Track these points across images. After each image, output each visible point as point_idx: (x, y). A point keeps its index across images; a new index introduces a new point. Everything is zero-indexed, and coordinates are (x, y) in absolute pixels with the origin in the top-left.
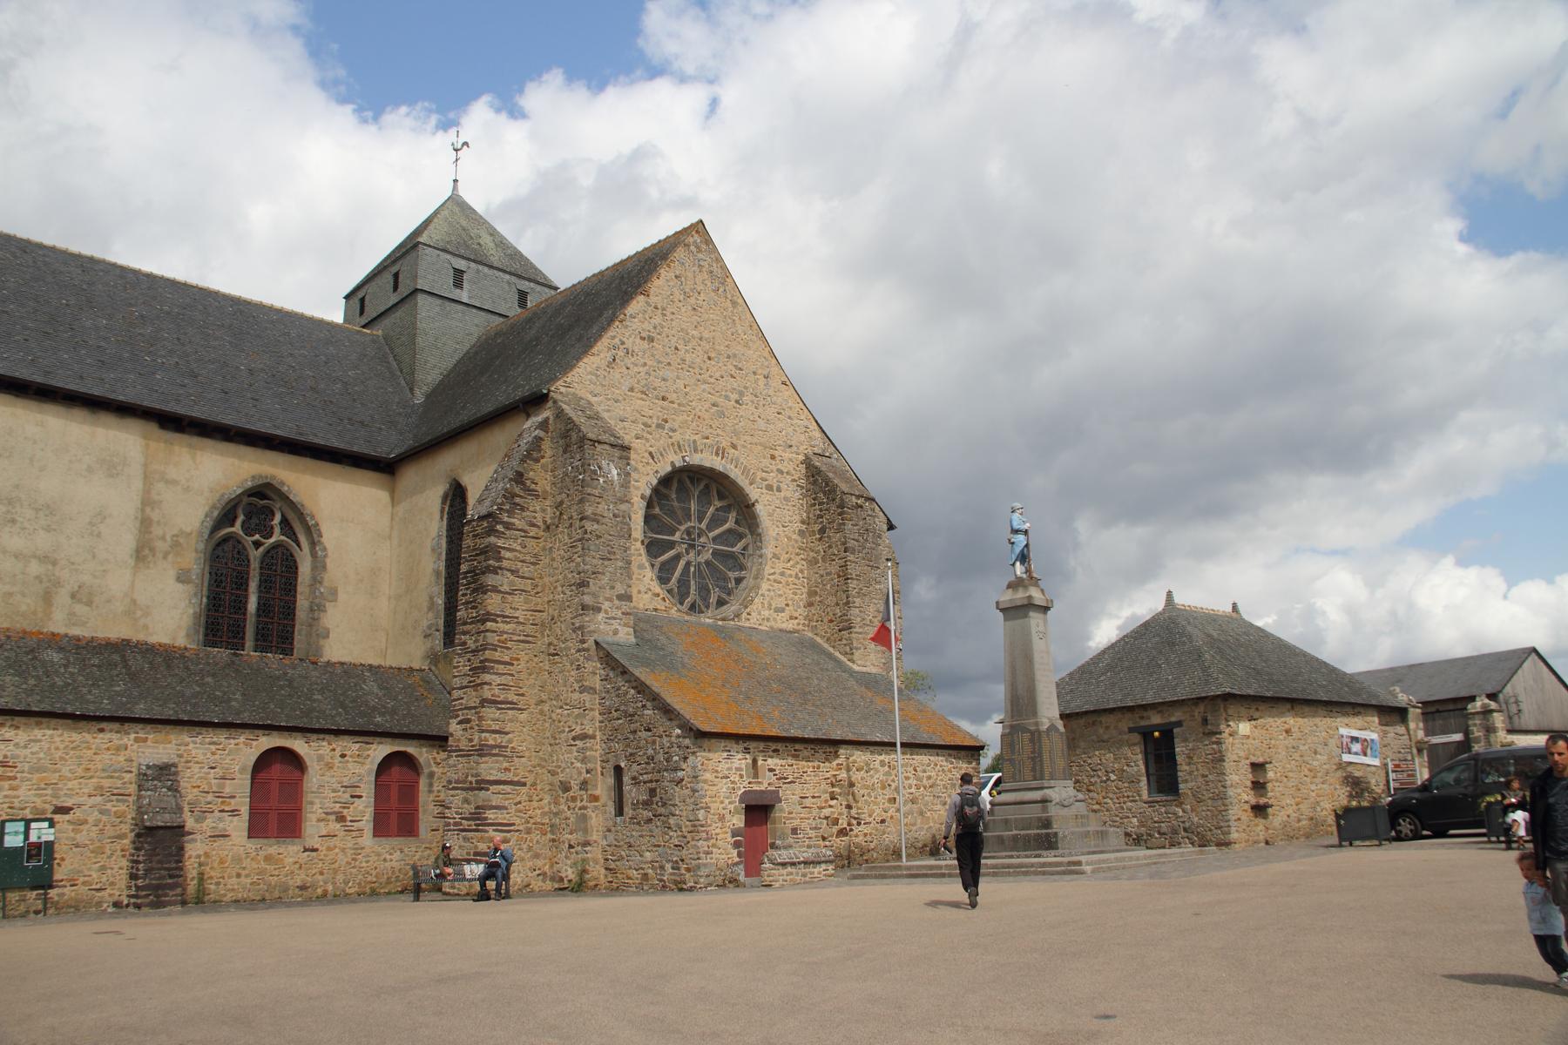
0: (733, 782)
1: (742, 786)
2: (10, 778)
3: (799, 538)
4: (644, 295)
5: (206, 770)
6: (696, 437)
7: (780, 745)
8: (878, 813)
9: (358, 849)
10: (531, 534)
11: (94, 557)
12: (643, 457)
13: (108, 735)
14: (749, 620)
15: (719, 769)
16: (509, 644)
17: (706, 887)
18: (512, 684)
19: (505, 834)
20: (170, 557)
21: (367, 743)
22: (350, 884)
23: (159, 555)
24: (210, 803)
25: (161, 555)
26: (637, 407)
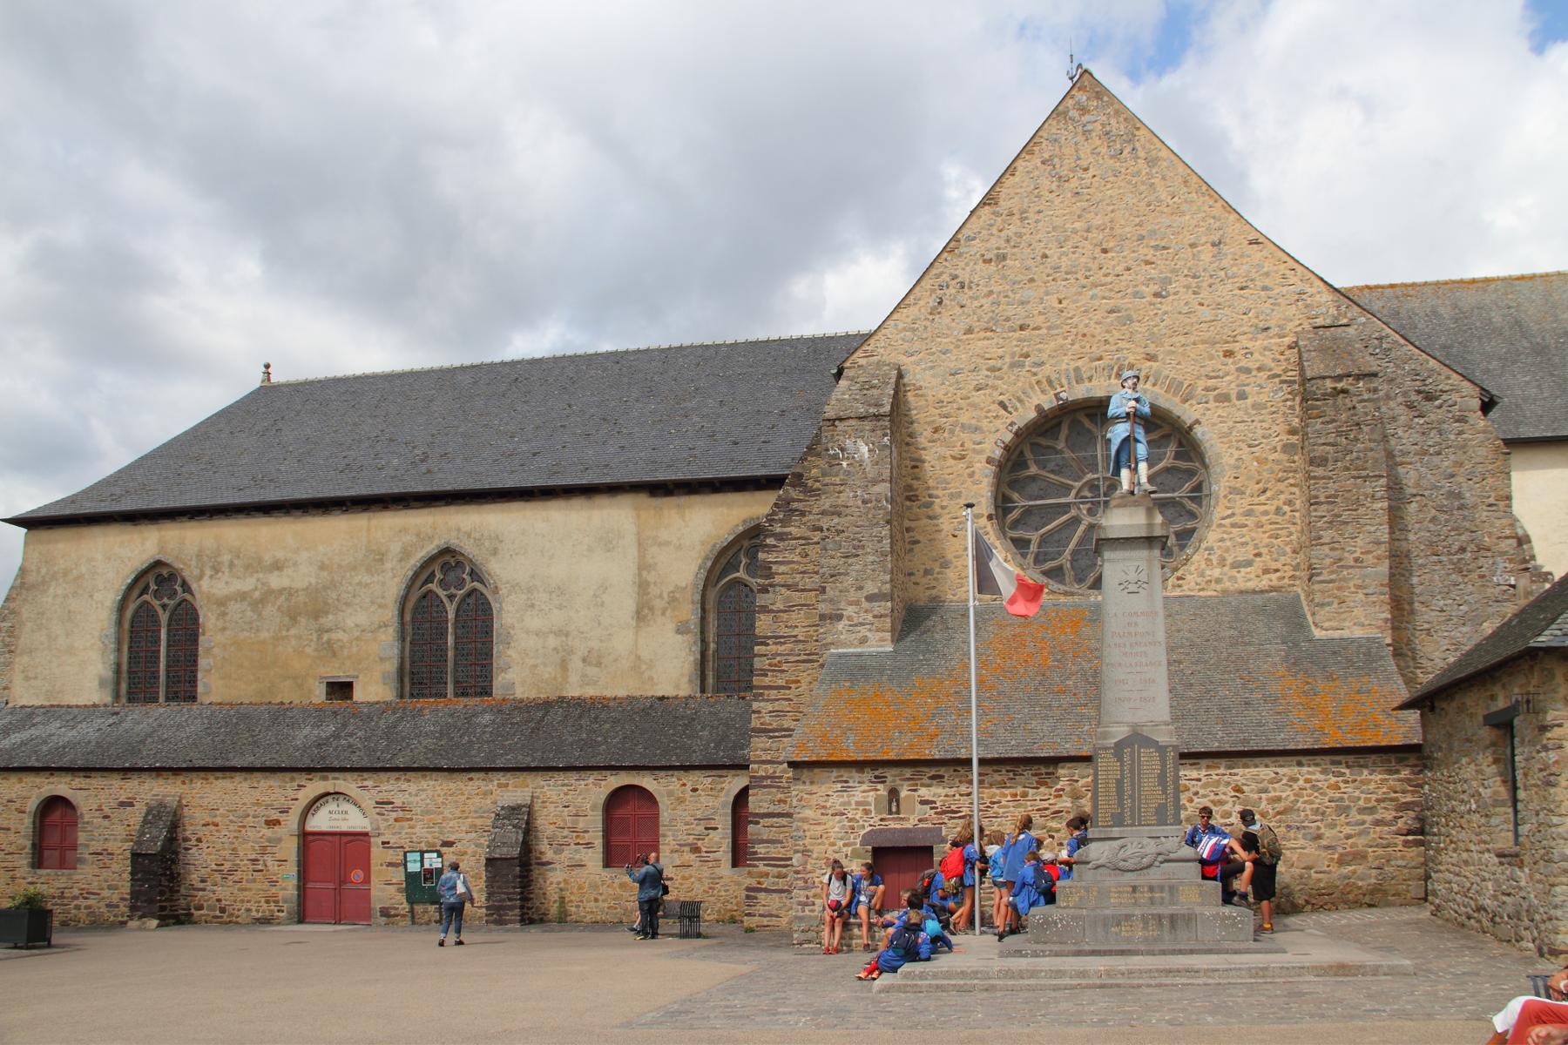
0: (851, 820)
2: (408, 820)
3: (1285, 457)
4: (989, 204)
5: (560, 809)
6: (1079, 363)
9: (716, 879)
10: (816, 540)
11: (599, 624)
12: (989, 411)
13: (476, 783)
14: (1180, 586)
15: (828, 804)
16: (784, 667)
17: (801, 944)
18: (788, 709)
19: (780, 869)
20: (668, 613)
21: (721, 776)
22: (709, 912)
23: (658, 613)
24: (565, 837)
25: (660, 613)
26: (978, 351)
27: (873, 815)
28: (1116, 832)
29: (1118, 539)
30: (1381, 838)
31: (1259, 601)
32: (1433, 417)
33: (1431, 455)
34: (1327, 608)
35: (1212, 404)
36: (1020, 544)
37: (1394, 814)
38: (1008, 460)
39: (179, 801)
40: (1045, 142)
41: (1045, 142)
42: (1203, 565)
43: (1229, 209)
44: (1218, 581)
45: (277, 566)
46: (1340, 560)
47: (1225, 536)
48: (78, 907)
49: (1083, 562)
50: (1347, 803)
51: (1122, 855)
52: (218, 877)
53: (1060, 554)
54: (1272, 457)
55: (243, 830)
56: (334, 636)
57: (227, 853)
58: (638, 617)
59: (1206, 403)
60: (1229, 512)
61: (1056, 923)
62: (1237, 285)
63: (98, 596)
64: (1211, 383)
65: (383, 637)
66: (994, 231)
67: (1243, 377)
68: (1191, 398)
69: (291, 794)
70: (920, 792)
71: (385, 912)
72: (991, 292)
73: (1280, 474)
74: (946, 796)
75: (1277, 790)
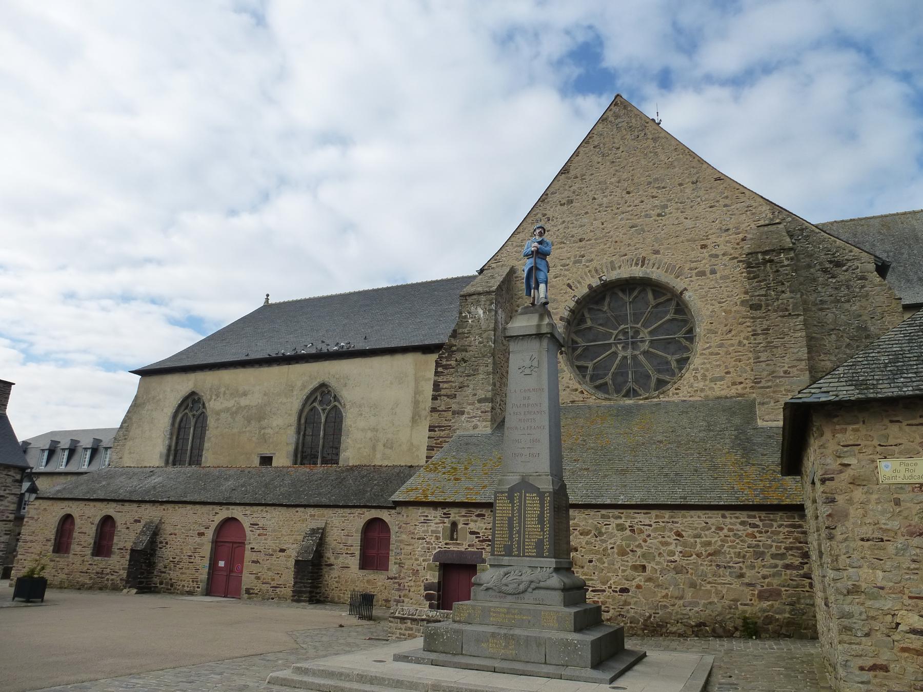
0: (428, 543)
1: (437, 546)
4: (565, 173)
6: (614, 258)
7: (484, 510)
8: (616, 581)
12: (561, 290)
14: (677, 394)
24: (341, 549)
27: (441, 540)
28: (506, 560)
29: (517, 336)
30: (791, 580)
31: (728, 403)
32: (842, 278)
33: (842, 302)
34: (766, 406)
35: (694, 278)
36: (582, 369)
37: (800, 560)
38: (574, 319)
39: (160, 520)
40: (595, 136)
41: (595, 136)
42: (692, 380)
43: (702, 161)
44: (702, 390)
45: (245, 394)
46: (773, 372)
47: (706, 361)
48: (108, 580)
49: (620, 379)
50: (762, 549)
51: (504, 581)
52: (172, 565)
53: (606, 375)
54: (733, 310)
55: (187, 538)
56: (266, 431)
57: (178, 551)
58: (413, 421)
59: (691, 277)
60: (708, 345)
61: (443, 636)
62: (708, 205)
63: (165, 410)
64: (693, 265)
65: (289, 432)
66: (567, 187)
67: (713, 260)
68: (681, 275)
69: (211, 517)
70: (470, 526)
71: (248, 591)
72: (564, 222)
73: (740, 320)
74: (486, 529)
75: (707, 536)
